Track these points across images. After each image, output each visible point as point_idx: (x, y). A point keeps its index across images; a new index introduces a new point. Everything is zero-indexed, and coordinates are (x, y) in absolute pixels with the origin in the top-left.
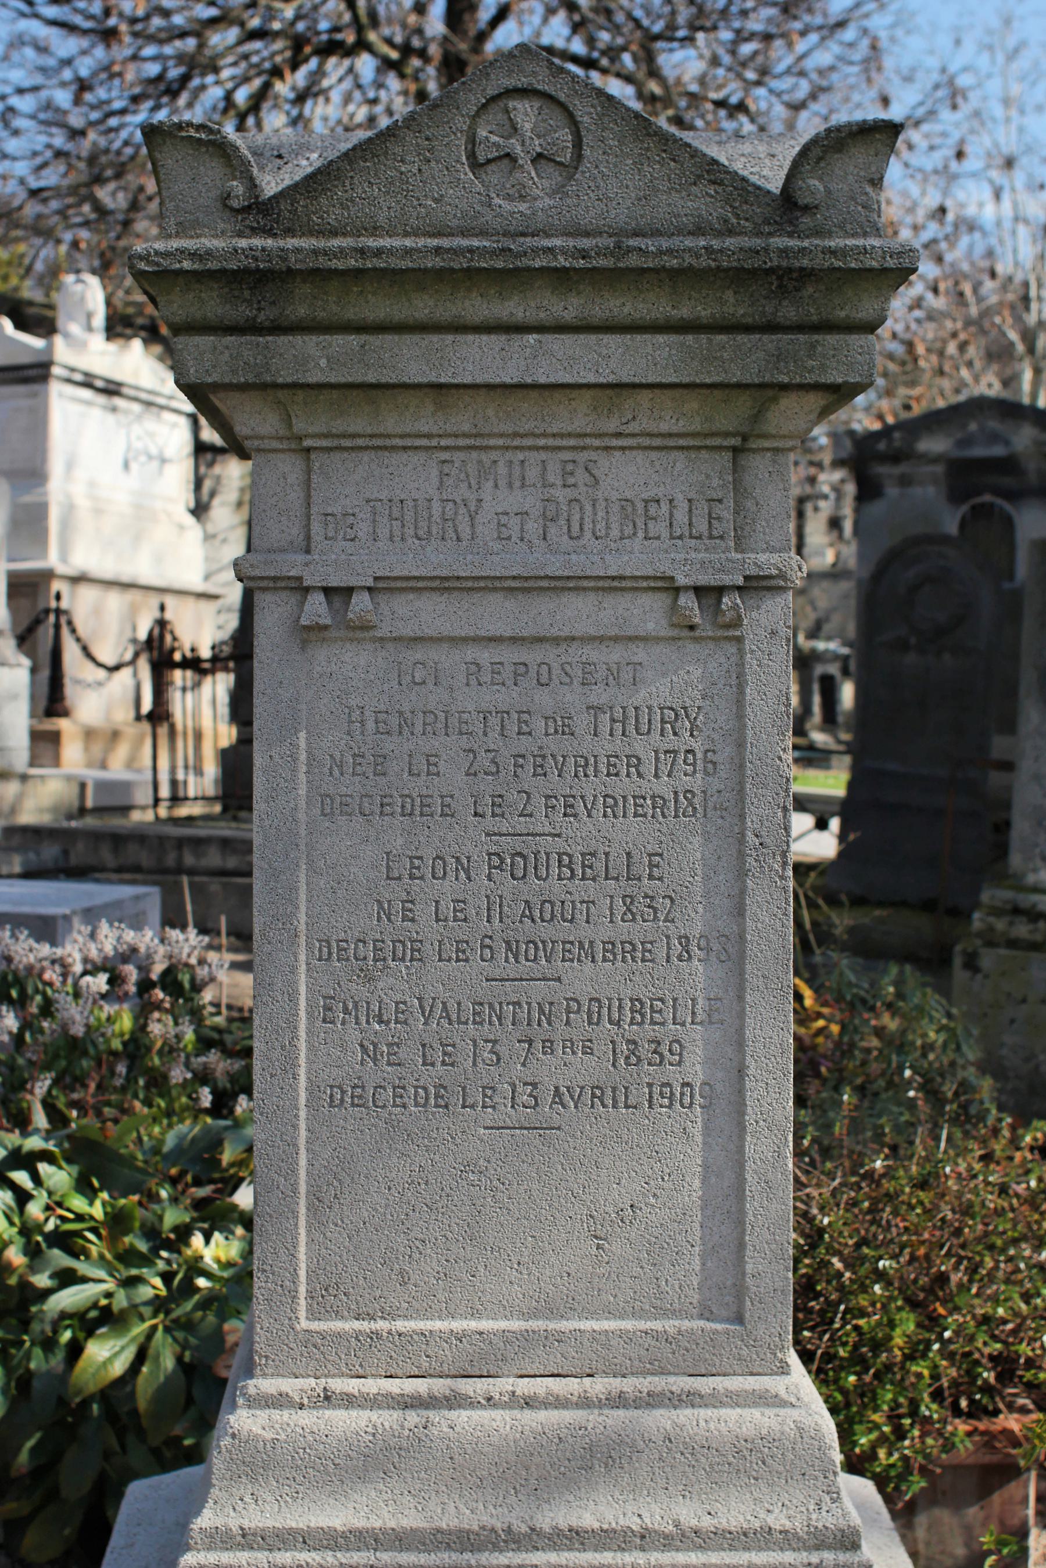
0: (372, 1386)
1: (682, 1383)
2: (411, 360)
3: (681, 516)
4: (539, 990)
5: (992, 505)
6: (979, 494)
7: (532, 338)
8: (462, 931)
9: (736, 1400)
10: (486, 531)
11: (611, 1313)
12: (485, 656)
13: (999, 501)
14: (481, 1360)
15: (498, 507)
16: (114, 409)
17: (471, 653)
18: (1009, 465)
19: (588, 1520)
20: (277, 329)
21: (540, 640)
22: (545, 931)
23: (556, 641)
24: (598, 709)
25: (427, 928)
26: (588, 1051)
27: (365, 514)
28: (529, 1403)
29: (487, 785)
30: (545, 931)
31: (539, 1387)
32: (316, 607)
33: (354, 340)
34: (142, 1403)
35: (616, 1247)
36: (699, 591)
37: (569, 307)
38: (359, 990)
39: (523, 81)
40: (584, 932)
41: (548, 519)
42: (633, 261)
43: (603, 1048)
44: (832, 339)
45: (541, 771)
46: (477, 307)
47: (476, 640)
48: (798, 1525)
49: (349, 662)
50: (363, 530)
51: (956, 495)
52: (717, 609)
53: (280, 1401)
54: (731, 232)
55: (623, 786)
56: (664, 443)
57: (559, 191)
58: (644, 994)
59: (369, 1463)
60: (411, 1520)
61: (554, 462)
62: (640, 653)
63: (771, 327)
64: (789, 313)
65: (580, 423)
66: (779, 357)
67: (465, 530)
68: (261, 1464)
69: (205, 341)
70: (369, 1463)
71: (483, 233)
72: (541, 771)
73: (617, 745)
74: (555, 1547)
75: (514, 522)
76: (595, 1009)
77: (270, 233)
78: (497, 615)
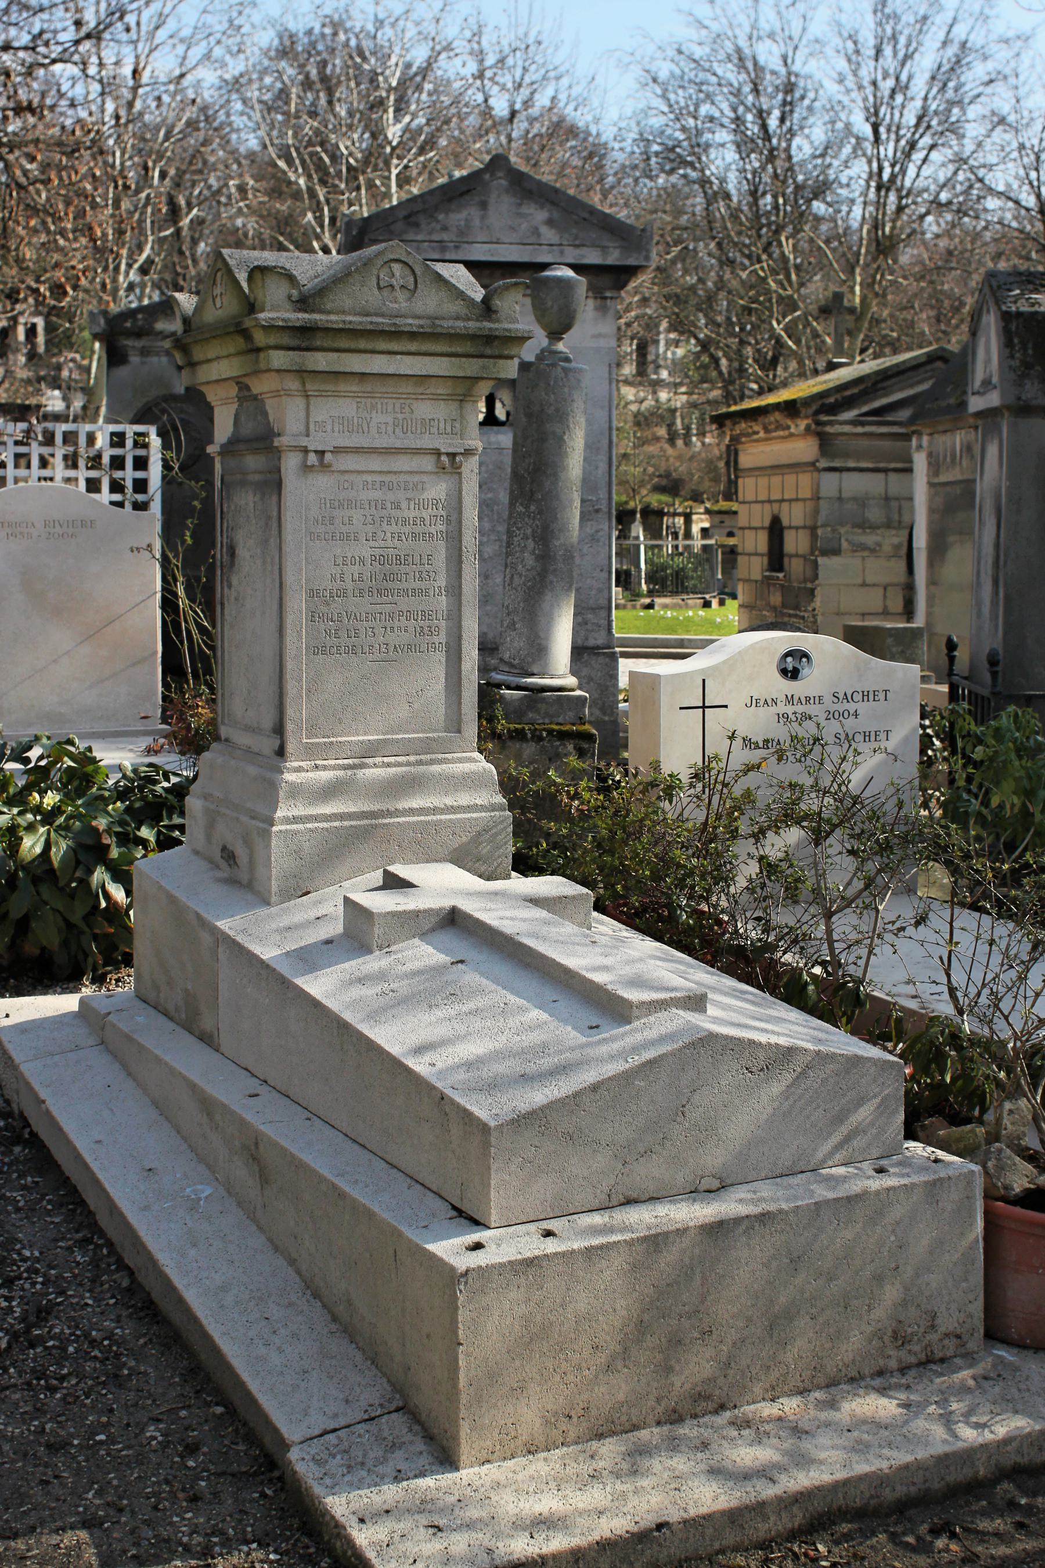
0: (332, 762)
1: (440, 756)
2: (356, 363)
3: (442, 425)
7: (399, 357)
8: (361, 585)
9: (460, 760)
10: (374, 430)
11: (414, 732)
12: (369, 478)
14: (370, 751)
15: (379, 421)
17: (365, 477)
19: (415, 805)
20: (308, 349)
22: (391, 585)
23: (395, 473)
24: (409, 499)
25: (349, 585)
26: (406, 631)
27: (330, 422)
28: (389, 765)
29: (370, 529)
30: (391, 585)
31: (392, 759)
32: (312, 458)
33: (335, 355)
34: (56, 864)
35: (416, 706)
36: (448, 454)
37: (413, 347)
38: (324, 609)
39: (396, 257)
40: (404, 585)
41: (395, 426)
42: (439, 330)
43: (411, 630)
44: (501, 362)
45: (389, 523)
46: (382, 345)
48: (486, 802)
49: (322, 482)
50: (329, 428)
53: (299, 770)
54: (469, 319)
55: (418, 529)
56: (436, 398)
57: (409, 299)
58: (426, 609)
59: (330, 792)
60: (353, 809)
61: (398, 403)
62: (425, 478)
63: (481, 356)
64: (488, 351)
65: (410, 390)
66: (484, 367)
67: (366, 429)
68: (296, 792)
69: (281, 353)
70: (330, 792)
71: (383, 315)
72: (389, 523)
73: (417, 513)
74: (404, 816)
76: (409, 614)
77: (306, 311)
78: (375, 463)
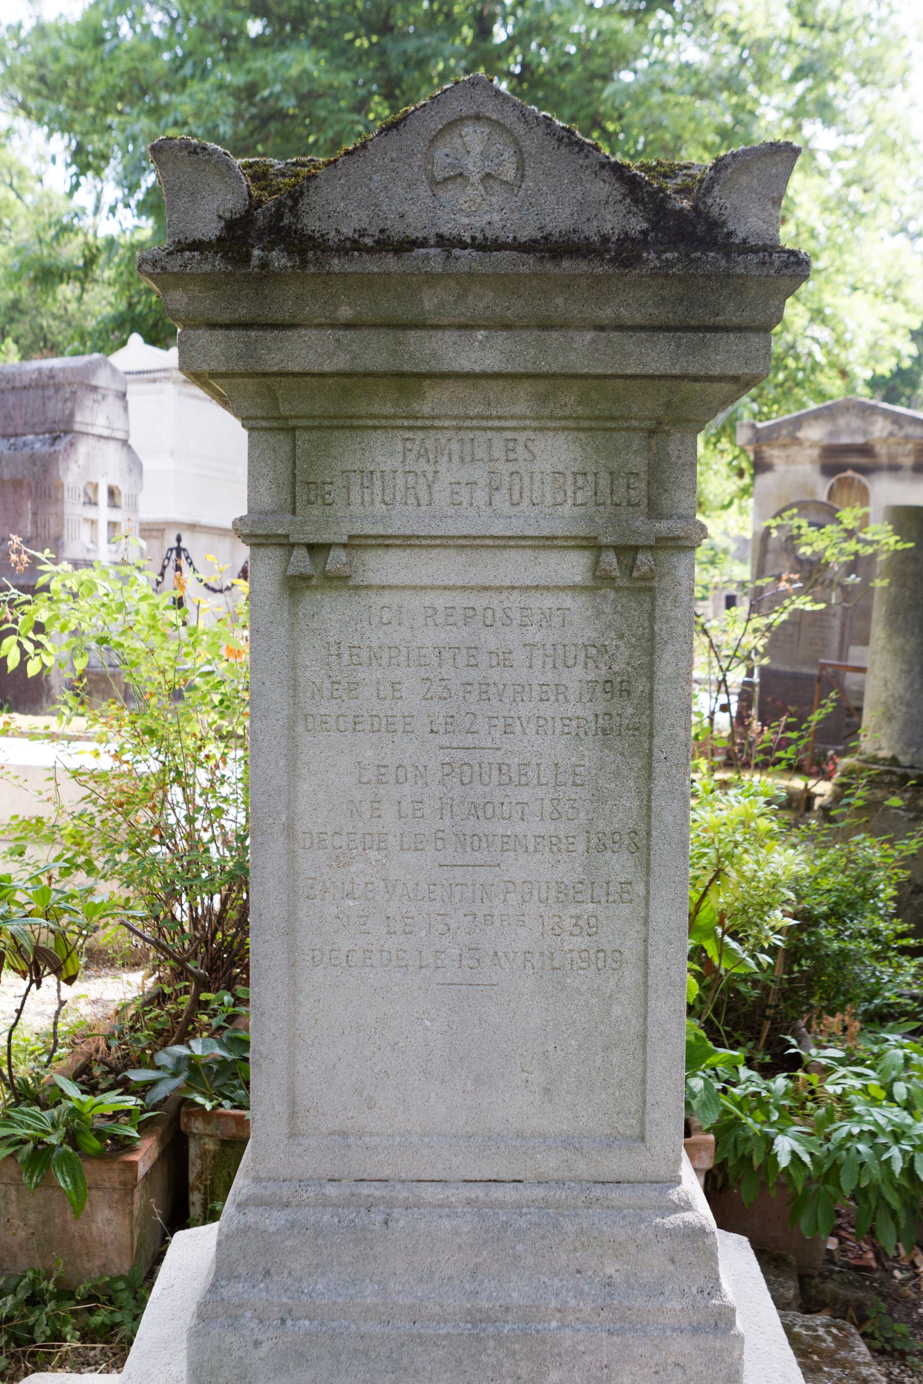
12: (441, 601)
13: (858, 476)
18: (866, 450)
21: (486, 588)
47: (433, 588)
51: (828, 470)
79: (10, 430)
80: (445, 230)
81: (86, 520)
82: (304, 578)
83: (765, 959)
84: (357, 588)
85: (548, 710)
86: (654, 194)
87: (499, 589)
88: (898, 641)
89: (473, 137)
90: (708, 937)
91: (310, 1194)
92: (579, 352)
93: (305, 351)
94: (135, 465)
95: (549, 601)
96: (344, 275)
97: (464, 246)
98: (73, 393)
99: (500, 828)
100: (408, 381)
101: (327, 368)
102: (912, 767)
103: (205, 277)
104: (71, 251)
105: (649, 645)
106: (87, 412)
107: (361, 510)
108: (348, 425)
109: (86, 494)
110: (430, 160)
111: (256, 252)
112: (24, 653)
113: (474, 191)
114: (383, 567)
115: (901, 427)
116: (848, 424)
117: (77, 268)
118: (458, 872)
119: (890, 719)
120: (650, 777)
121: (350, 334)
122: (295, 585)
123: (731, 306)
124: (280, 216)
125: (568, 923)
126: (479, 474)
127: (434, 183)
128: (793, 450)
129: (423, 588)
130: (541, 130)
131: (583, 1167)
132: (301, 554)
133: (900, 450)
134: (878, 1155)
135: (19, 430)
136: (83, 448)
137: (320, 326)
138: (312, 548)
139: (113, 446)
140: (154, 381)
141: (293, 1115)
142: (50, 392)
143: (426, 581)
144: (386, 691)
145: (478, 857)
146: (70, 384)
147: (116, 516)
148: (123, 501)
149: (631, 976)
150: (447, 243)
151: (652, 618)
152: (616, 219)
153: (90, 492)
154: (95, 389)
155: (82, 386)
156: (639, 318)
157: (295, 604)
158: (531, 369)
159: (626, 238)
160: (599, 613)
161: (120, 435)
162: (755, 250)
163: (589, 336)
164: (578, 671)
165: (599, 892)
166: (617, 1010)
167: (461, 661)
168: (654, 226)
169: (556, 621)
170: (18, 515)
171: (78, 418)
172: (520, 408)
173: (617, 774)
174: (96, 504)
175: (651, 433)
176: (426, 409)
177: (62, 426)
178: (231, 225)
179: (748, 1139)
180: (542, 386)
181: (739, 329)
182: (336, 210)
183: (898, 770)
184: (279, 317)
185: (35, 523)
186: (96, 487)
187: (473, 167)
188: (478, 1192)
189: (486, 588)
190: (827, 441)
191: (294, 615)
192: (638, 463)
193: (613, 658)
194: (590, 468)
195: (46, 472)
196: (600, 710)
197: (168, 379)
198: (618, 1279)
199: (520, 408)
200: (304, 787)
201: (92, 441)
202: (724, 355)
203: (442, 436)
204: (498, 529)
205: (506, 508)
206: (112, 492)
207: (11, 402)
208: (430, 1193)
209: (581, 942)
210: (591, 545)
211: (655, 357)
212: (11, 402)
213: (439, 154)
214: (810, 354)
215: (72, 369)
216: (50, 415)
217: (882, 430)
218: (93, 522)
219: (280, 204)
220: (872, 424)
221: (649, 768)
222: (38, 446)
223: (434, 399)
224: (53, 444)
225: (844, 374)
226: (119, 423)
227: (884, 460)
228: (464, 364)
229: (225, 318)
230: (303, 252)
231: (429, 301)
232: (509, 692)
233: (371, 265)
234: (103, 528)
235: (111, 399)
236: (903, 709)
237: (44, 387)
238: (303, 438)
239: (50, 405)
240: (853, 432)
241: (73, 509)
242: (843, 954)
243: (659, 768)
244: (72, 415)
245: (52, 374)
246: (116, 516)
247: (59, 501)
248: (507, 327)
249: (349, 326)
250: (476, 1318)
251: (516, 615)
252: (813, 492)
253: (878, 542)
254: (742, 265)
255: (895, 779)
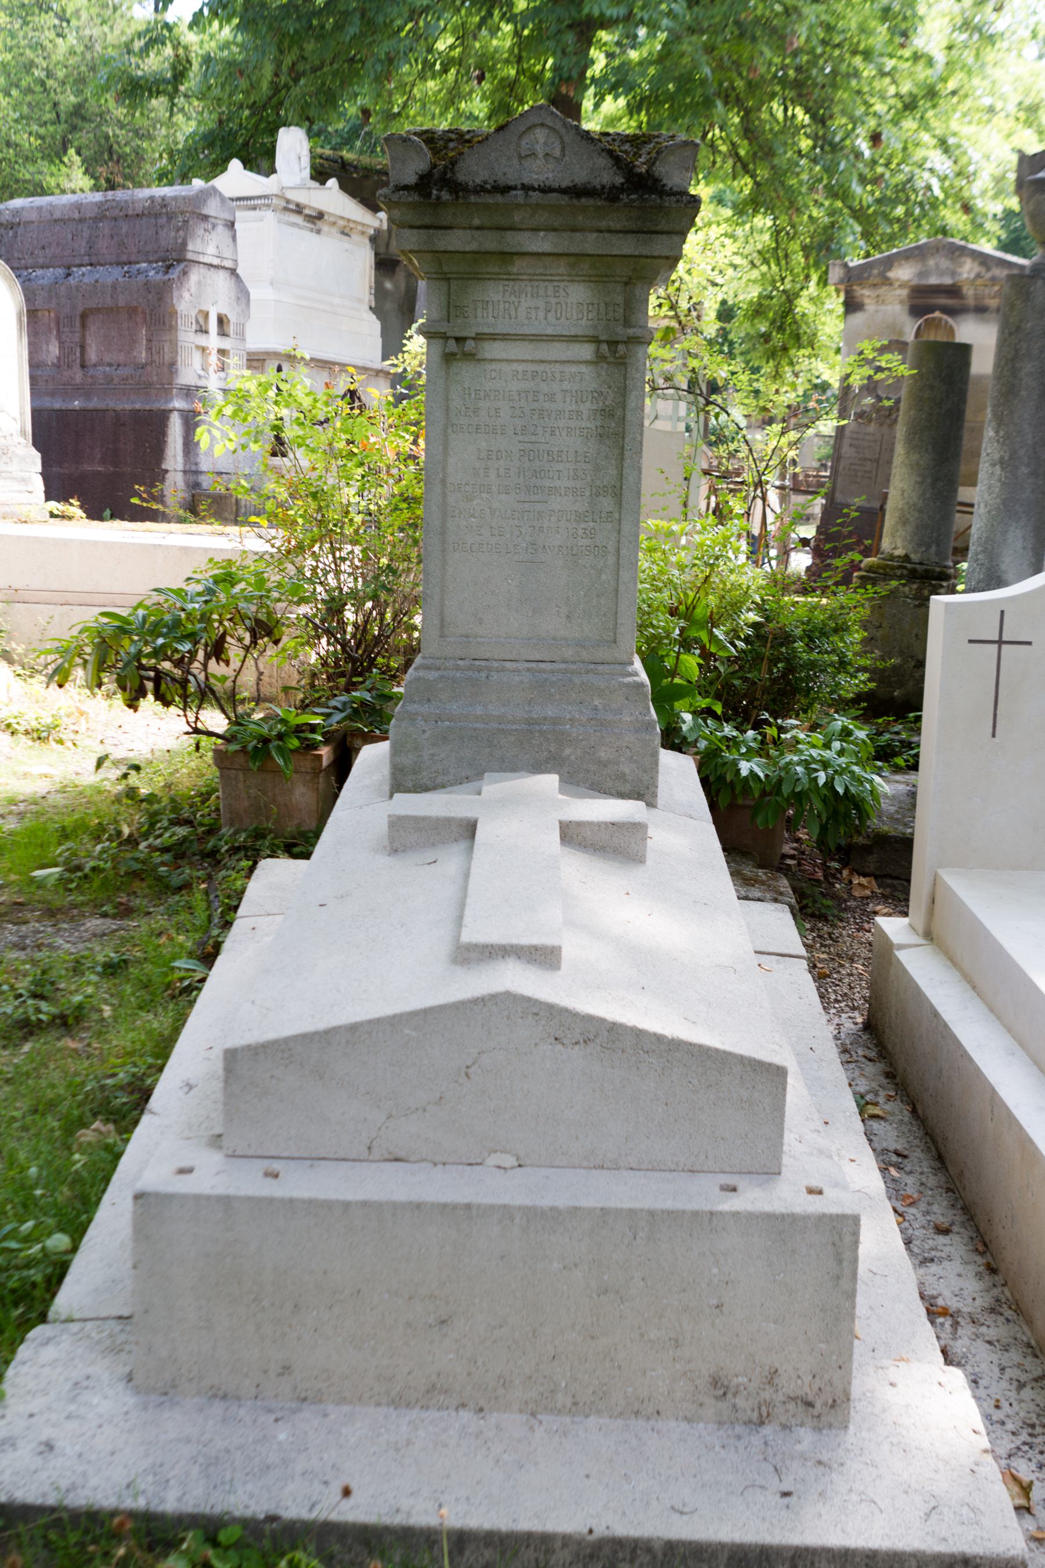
4: (538, 507)
5: (940, 319)
6: (933, 312)
12: (521, 367)
13: (945, 317)
16: (319, 232)
18: (953, 291)
21: (543, 362)
47: (517, 361)
51: (916, 311)
52: (615, 352)
75: (533, 312)
79: (124, 258)
80: (525, 181)
81: (197, 347)
82: (453, 355)
83: (740, 644)
84: (479, 360)
85: (572, 424)
86: (627, 165)
87: (550, 362)
88: (915, 457)
89: (540, 134)
90: (702, 628)
91: (450, 664)
92: (590, 243)
93: (457, 240)
94: (242, 294)
95: (574, 369)
96: (476, 204)
97: (534, 189)
98: (186, 222)
99: (548, 483)
100: (506, 256)
101: (467, 249)
102: (921, 563)
103: (410, 203)
104: (156, 63)
105: (623, 392)
106: (199, 240)
107: (484, 321)
108: (476, 277)
109: (197, 322)
110: (518, 145)
111: (435, 192)
112: (213, 438)
113: (540, 162)
114: (492, 350)
115: (988, 269)
116: (937, 265)
117: (165, 81)
118: (526, 505)
119: (905, 524)
120: (622, 459)
121: (479, 232)
122: (449, 358)
123: (663, 222)
124: (445, 173)
125: (580, 532)
126: (540, 303)
127: (520, 157)
128: (883, 290)
129: (512, 361)
130: (573, 132)
131: (585, 655)
132: (452, 342)
133: (987, 291)
134: (809, 775)
135: (133, 258)
136: (195, 276)
137: (464, 228)
138: (458, 340)
139: (222, 275)
140: (254, 208)
141: (442, 626)
142: (163, 220)
143: (514, 358)
144: (493, 412)
145: (536, 498)
146: (182, 213)
147: (226, 344)
148: (231, 329)
149: (611, 559)
150: (526, 188)
151: (625, 378)
152: (608, 177)
153: (201, 320)
154: (205, 218)
155: (190, 215)
156: (618, 227)
157: (448, 368)
158: (566, 251)
159: (613, 187)
160: (599, 375)
161: (228, 264)
162: (675, 194)
163: (595, 235)
164: (588, 405)
165: (596, 517)
166: (604, 577)
167: (530, 398)
168: (628, 181)
169: (578, 378)
170: (134, 341)
171: (190, 247)
172: (561, 270)
173: (606, 457)
174: (207, 332)
175: (626, 284)
176: (515, 270)
177: (174, 255)
178: (422, 177)
179: (725, 764)
180: (572, 260)
181: (668, 233)
182: (474, 170)
183: (909, 566)
184: (444, 223)
185: (149, 349)
186: (206, 315)
187: (540, 150)
188: (534, 665)
189: (543, 362)
190: (915, 282)
191: (447, 373)
192: (620, 299)
193: (606, 398)
194: (596, 301)
195: (160, 299)
196: (599, 424)
197: (268, 206)
198: (600, 707)
199: (561, 270)
200: (451, 461)
201: (202, 270)
202: (659, 246)
203: (523, 284)
204: (549, 331)
205: (553, 321)
206: (221, 321)
207: (124, 230)
208: (508, 665)
209: (587, 542)
210: (596, 340)
211: (627, 246)
212: (124, 230)
213: (523, 143)
214: (929, 188)
215: (184, 198)
216: (163, 243)
217: (969, 272)
218: (203, 349)
219: (445, 167)
220: (961, 265)
221: (622, 454)
222: (152, 273)
223: (519, 266)
224: (167, 273)
225: (967, 208)
226: (227, 253)
227: (971, 302)
228: (534, 248)
229: (418, 223)
230: (457, 193)
231: (517, 217)
232: (554, 415)
233: (489, 199)
234: (213, 359)
235: (220, 229)
236: (916, 514)
237: (157, 216)
238: (454, 284)
239: (163, 234)
240: (942, 273)
241: (187, 336)
242: (812, 665)
243: (627, 454)
244: (184, 244)
245: (164, 202)
246: (226, 344)
247: (173, 328)
248: (555, 230)
249: (479, 228)
250: (530, 722)
251: (558, 375)
252: (901, 333)
253: (889, 369)
254: (669, 202)
255: (905, 572)
